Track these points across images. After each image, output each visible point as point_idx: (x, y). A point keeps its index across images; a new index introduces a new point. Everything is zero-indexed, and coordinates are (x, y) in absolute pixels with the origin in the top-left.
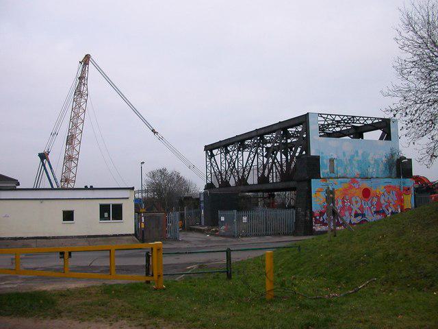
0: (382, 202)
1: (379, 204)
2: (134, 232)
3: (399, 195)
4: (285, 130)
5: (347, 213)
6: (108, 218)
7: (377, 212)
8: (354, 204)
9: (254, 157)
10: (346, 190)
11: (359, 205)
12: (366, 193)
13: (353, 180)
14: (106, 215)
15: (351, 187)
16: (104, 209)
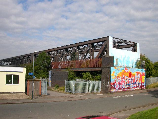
0: (135, 79)
1: (134, 80)
2: (24, 91)
3: (141, 76)
4: (92, 44)
5: (123, 84)
6: (11, 83)
7: (134, 83)
8: (126, 79)
9: (127, 44)
10: (123, 73)
11: (127, 80)
12: (130, 75)
13: (126, 68)
14: (10, 81)
15: (125, 72)
16: (9, 77)
